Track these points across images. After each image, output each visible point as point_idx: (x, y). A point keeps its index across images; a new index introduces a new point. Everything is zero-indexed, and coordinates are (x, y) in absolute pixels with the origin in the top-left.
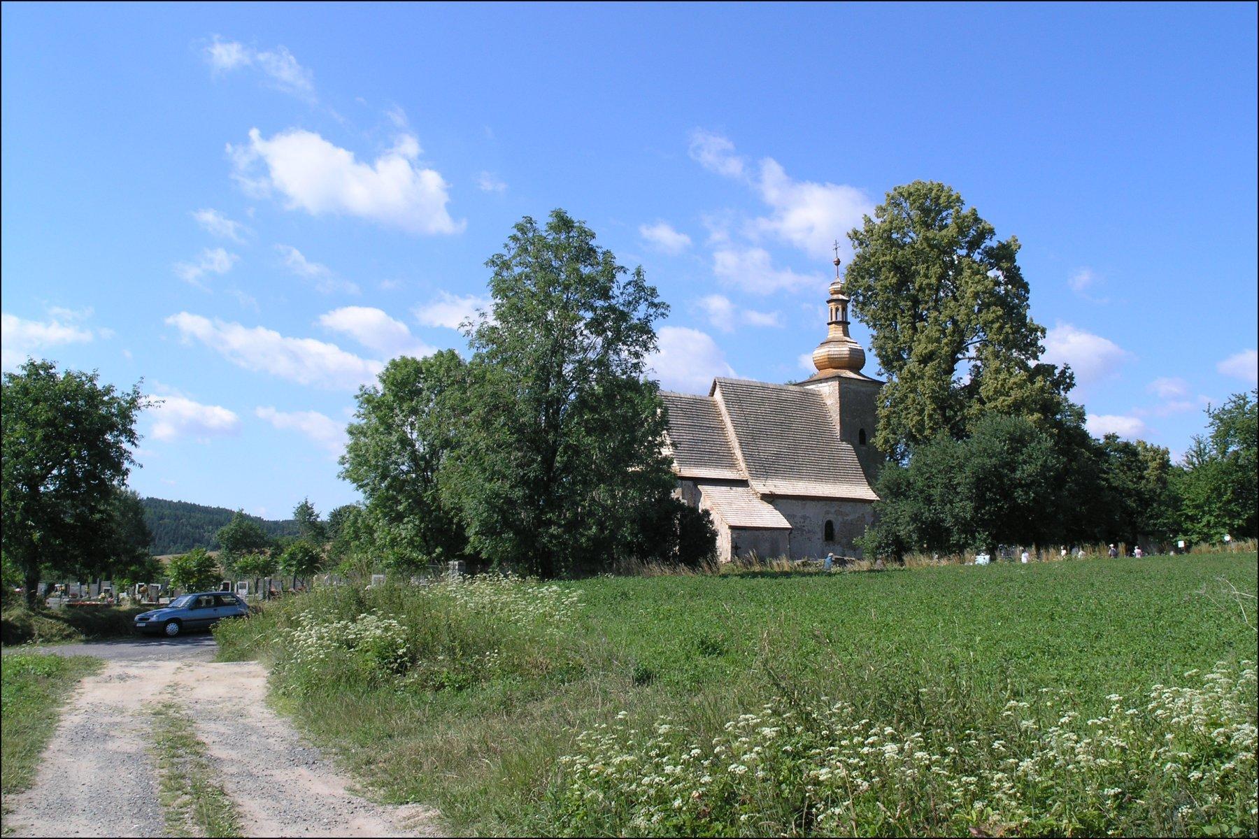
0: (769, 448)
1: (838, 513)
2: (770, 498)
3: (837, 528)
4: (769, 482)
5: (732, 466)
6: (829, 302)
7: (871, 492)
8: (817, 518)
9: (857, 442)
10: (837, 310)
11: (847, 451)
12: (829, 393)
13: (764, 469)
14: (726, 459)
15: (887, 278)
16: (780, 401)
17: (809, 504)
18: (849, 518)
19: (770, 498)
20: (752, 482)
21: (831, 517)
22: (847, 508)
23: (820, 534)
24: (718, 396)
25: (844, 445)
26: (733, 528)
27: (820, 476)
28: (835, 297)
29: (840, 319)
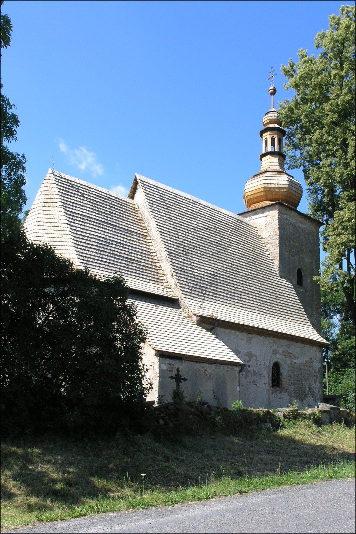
0: (205, 267)
1: (287, 354)
2: (209, 323)
3: (284, 371)
4: (206, 304)
5: (157, 280)
6: (262, 133)
7: (227, 349)
8: (264, 354)
9: (295, 281)
10: (273, 140)
11: (287, 289)
12: (267, 225)
13: (201, 288)
14: (153, 271)
15: (338, 96)
16: (212, 220)
17: (256, 339)
18: (298, 361)
19: (209, 323)
20: (184, 301)
21: (278, 358)
22: (296, 349)
23: (267, 378)
24: (140, 197)
25: (283, 281)
26: (162, 355)
27: (264, 308)
28: (271, 125)
29: (277, 149)
